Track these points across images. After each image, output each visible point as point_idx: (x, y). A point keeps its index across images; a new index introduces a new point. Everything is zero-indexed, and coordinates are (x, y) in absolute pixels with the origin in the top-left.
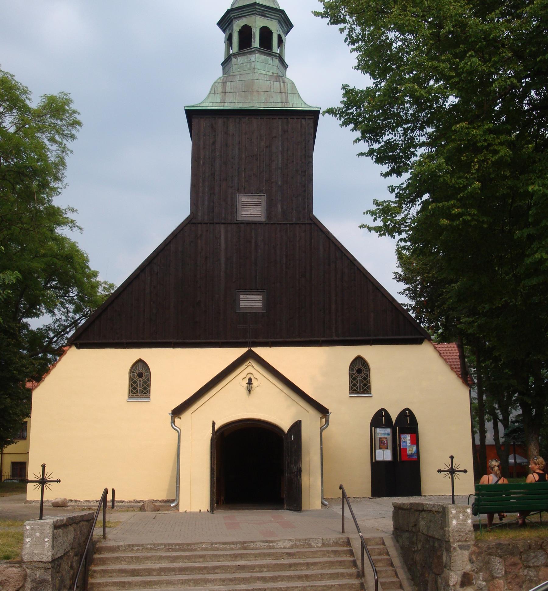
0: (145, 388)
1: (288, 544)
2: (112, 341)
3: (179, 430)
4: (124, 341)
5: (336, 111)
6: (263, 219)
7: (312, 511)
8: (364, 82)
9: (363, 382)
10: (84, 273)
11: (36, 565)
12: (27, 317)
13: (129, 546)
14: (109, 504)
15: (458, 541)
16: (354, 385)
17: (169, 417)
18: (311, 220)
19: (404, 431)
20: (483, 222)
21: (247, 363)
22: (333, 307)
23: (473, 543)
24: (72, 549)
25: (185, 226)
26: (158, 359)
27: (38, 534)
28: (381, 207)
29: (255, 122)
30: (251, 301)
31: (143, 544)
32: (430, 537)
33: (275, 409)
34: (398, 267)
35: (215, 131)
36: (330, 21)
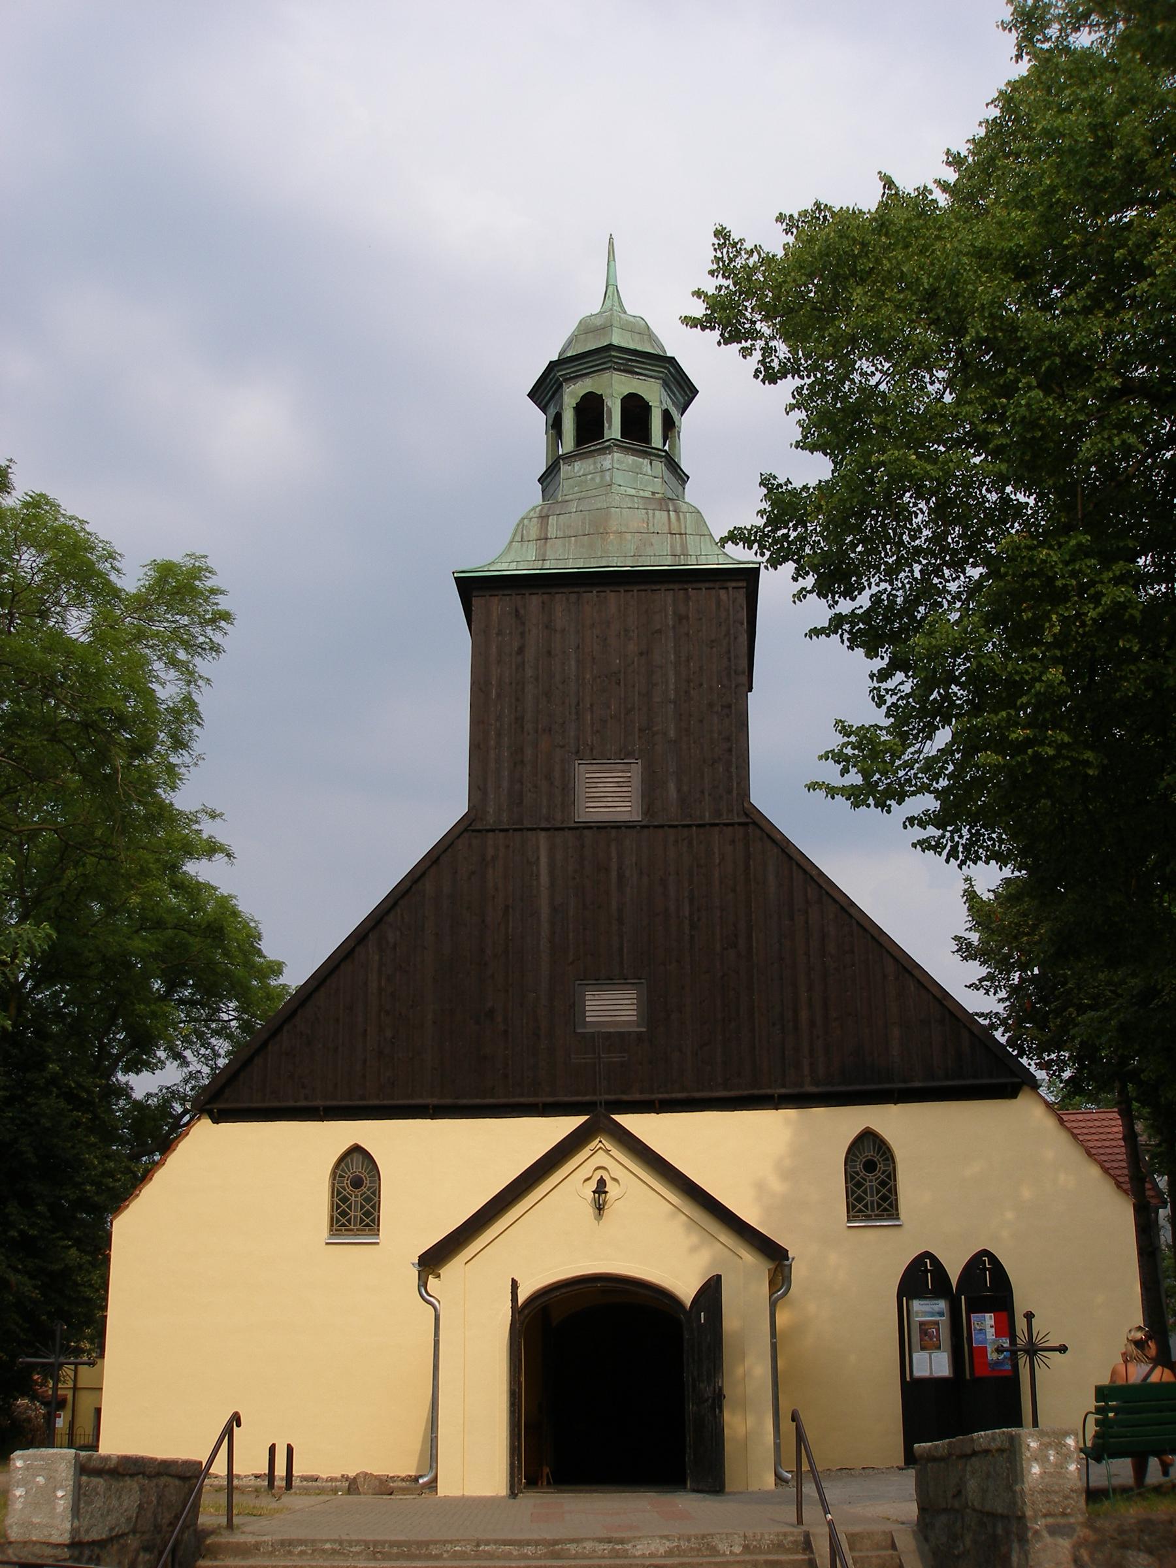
0: (368, 1214)
1: (661, 1547)
2: (291, 1104)
3: (436, 1303)
4: (319, 1103)
5: (750, 534)
6: (636, 817)
7: (752, 1493)
8: (812, 470)
9: (878, 1191)
10: (249, 965)
13: (283, 1543)
14: (280, 1483)
15: (1045, 1516)
18: (747, 815)
19: (978, 1306)
20: (1087, 763)
21: (594, 1144)
22: (804, 1015)
23: (1081, 1518)
24: (134, 1531)
25: (458, 837)
26: (392, 1141)
27: (40, 1480)
28: (853, 739)
29: (613, 600)
30: (612, 1007)
32: (988, 1514)
33: (665, 1254)
34: (970, 929)
35: (523, 624)
36: (722, 335)
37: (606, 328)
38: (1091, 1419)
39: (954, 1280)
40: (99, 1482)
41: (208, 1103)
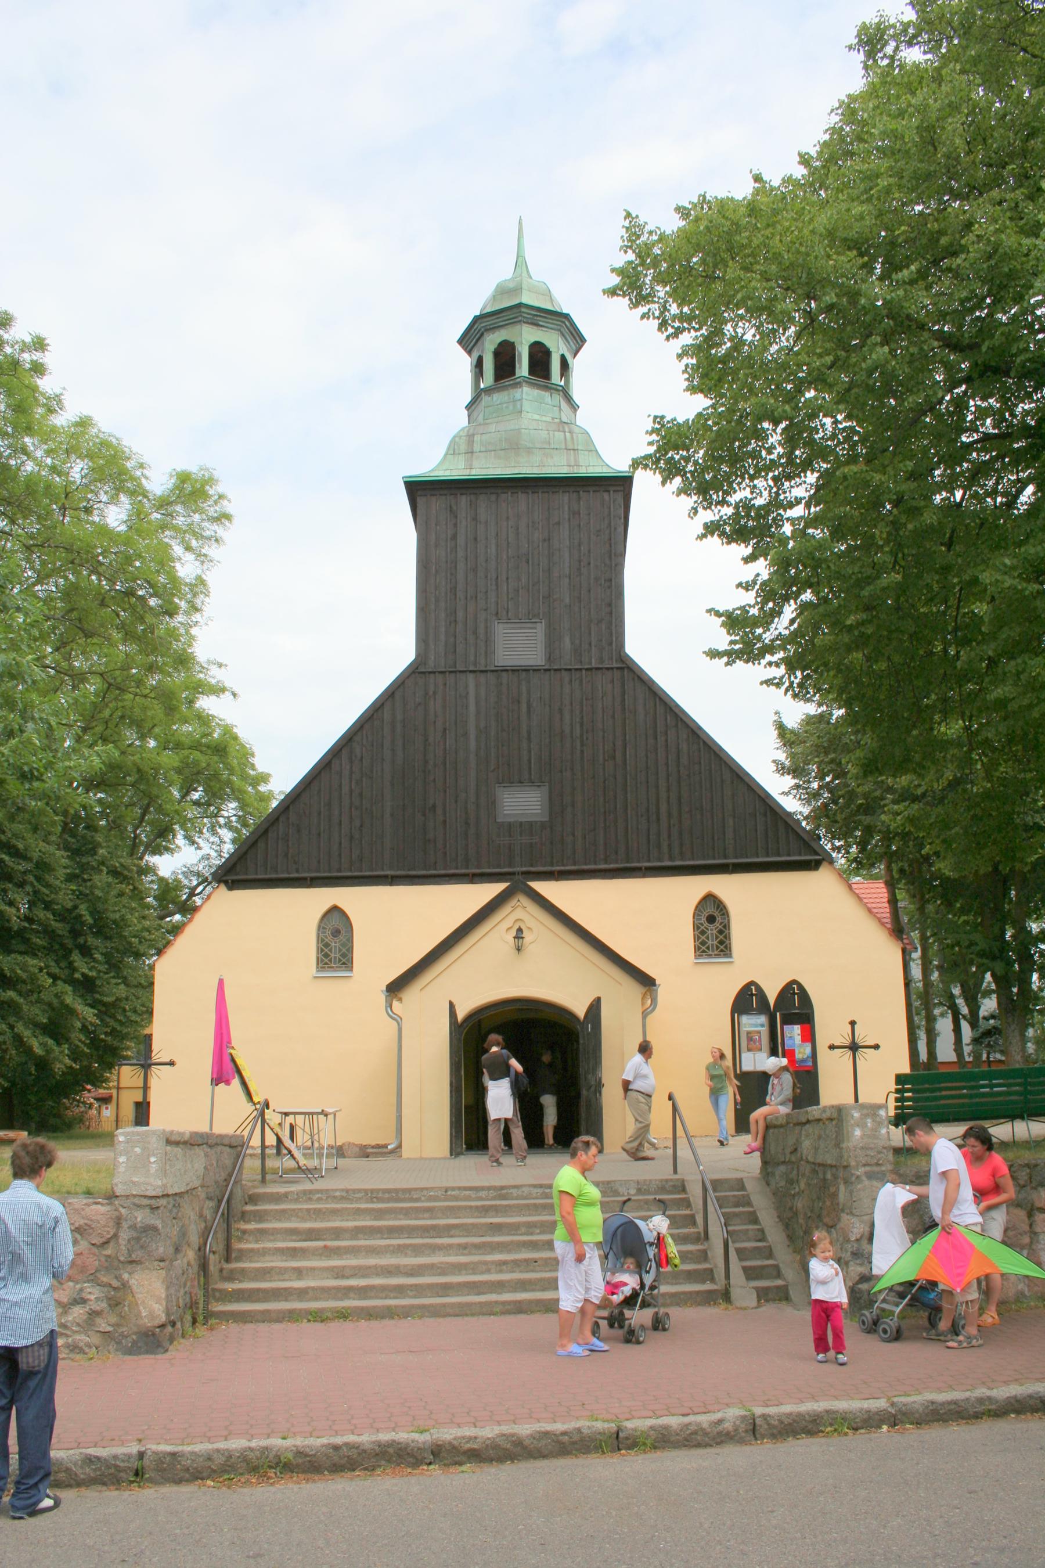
0: (344, 955)
9: (717, 937)
10: (245, 777)
11: (136, 1201)
12: (154, 853)
15: (864, 1165)
16: (703, 943)
17: (382, 998)
18: (623, 662)
19: (788, 1020)
21: (513, 902)
23: (890, 1167)
24: (202, 1186)
25: (408, 677)
26: (360, 902)
27: (138, 1150)
30: (522, 804)
31: (327, 1190)
32: (820, 1165)
33: (562, 981)
35: (456, 517)
37: (517, 290)
38: (892, 1096)
39: (772, 1002)
40: (178, 1150)
41: (225, 875)
